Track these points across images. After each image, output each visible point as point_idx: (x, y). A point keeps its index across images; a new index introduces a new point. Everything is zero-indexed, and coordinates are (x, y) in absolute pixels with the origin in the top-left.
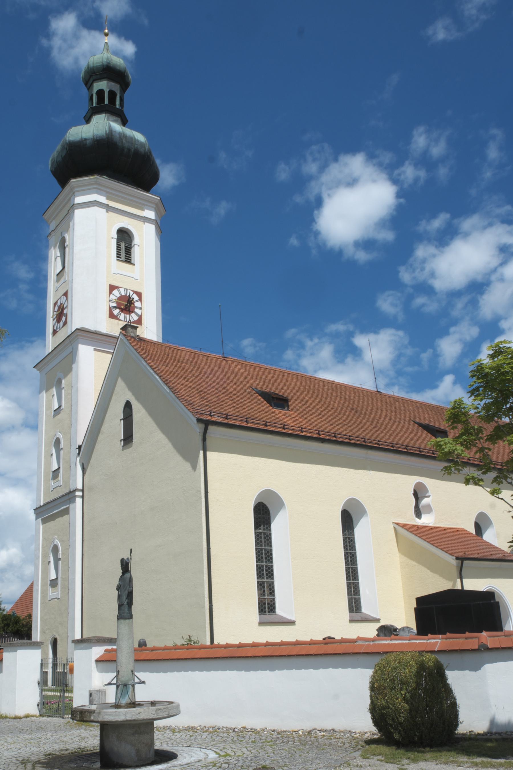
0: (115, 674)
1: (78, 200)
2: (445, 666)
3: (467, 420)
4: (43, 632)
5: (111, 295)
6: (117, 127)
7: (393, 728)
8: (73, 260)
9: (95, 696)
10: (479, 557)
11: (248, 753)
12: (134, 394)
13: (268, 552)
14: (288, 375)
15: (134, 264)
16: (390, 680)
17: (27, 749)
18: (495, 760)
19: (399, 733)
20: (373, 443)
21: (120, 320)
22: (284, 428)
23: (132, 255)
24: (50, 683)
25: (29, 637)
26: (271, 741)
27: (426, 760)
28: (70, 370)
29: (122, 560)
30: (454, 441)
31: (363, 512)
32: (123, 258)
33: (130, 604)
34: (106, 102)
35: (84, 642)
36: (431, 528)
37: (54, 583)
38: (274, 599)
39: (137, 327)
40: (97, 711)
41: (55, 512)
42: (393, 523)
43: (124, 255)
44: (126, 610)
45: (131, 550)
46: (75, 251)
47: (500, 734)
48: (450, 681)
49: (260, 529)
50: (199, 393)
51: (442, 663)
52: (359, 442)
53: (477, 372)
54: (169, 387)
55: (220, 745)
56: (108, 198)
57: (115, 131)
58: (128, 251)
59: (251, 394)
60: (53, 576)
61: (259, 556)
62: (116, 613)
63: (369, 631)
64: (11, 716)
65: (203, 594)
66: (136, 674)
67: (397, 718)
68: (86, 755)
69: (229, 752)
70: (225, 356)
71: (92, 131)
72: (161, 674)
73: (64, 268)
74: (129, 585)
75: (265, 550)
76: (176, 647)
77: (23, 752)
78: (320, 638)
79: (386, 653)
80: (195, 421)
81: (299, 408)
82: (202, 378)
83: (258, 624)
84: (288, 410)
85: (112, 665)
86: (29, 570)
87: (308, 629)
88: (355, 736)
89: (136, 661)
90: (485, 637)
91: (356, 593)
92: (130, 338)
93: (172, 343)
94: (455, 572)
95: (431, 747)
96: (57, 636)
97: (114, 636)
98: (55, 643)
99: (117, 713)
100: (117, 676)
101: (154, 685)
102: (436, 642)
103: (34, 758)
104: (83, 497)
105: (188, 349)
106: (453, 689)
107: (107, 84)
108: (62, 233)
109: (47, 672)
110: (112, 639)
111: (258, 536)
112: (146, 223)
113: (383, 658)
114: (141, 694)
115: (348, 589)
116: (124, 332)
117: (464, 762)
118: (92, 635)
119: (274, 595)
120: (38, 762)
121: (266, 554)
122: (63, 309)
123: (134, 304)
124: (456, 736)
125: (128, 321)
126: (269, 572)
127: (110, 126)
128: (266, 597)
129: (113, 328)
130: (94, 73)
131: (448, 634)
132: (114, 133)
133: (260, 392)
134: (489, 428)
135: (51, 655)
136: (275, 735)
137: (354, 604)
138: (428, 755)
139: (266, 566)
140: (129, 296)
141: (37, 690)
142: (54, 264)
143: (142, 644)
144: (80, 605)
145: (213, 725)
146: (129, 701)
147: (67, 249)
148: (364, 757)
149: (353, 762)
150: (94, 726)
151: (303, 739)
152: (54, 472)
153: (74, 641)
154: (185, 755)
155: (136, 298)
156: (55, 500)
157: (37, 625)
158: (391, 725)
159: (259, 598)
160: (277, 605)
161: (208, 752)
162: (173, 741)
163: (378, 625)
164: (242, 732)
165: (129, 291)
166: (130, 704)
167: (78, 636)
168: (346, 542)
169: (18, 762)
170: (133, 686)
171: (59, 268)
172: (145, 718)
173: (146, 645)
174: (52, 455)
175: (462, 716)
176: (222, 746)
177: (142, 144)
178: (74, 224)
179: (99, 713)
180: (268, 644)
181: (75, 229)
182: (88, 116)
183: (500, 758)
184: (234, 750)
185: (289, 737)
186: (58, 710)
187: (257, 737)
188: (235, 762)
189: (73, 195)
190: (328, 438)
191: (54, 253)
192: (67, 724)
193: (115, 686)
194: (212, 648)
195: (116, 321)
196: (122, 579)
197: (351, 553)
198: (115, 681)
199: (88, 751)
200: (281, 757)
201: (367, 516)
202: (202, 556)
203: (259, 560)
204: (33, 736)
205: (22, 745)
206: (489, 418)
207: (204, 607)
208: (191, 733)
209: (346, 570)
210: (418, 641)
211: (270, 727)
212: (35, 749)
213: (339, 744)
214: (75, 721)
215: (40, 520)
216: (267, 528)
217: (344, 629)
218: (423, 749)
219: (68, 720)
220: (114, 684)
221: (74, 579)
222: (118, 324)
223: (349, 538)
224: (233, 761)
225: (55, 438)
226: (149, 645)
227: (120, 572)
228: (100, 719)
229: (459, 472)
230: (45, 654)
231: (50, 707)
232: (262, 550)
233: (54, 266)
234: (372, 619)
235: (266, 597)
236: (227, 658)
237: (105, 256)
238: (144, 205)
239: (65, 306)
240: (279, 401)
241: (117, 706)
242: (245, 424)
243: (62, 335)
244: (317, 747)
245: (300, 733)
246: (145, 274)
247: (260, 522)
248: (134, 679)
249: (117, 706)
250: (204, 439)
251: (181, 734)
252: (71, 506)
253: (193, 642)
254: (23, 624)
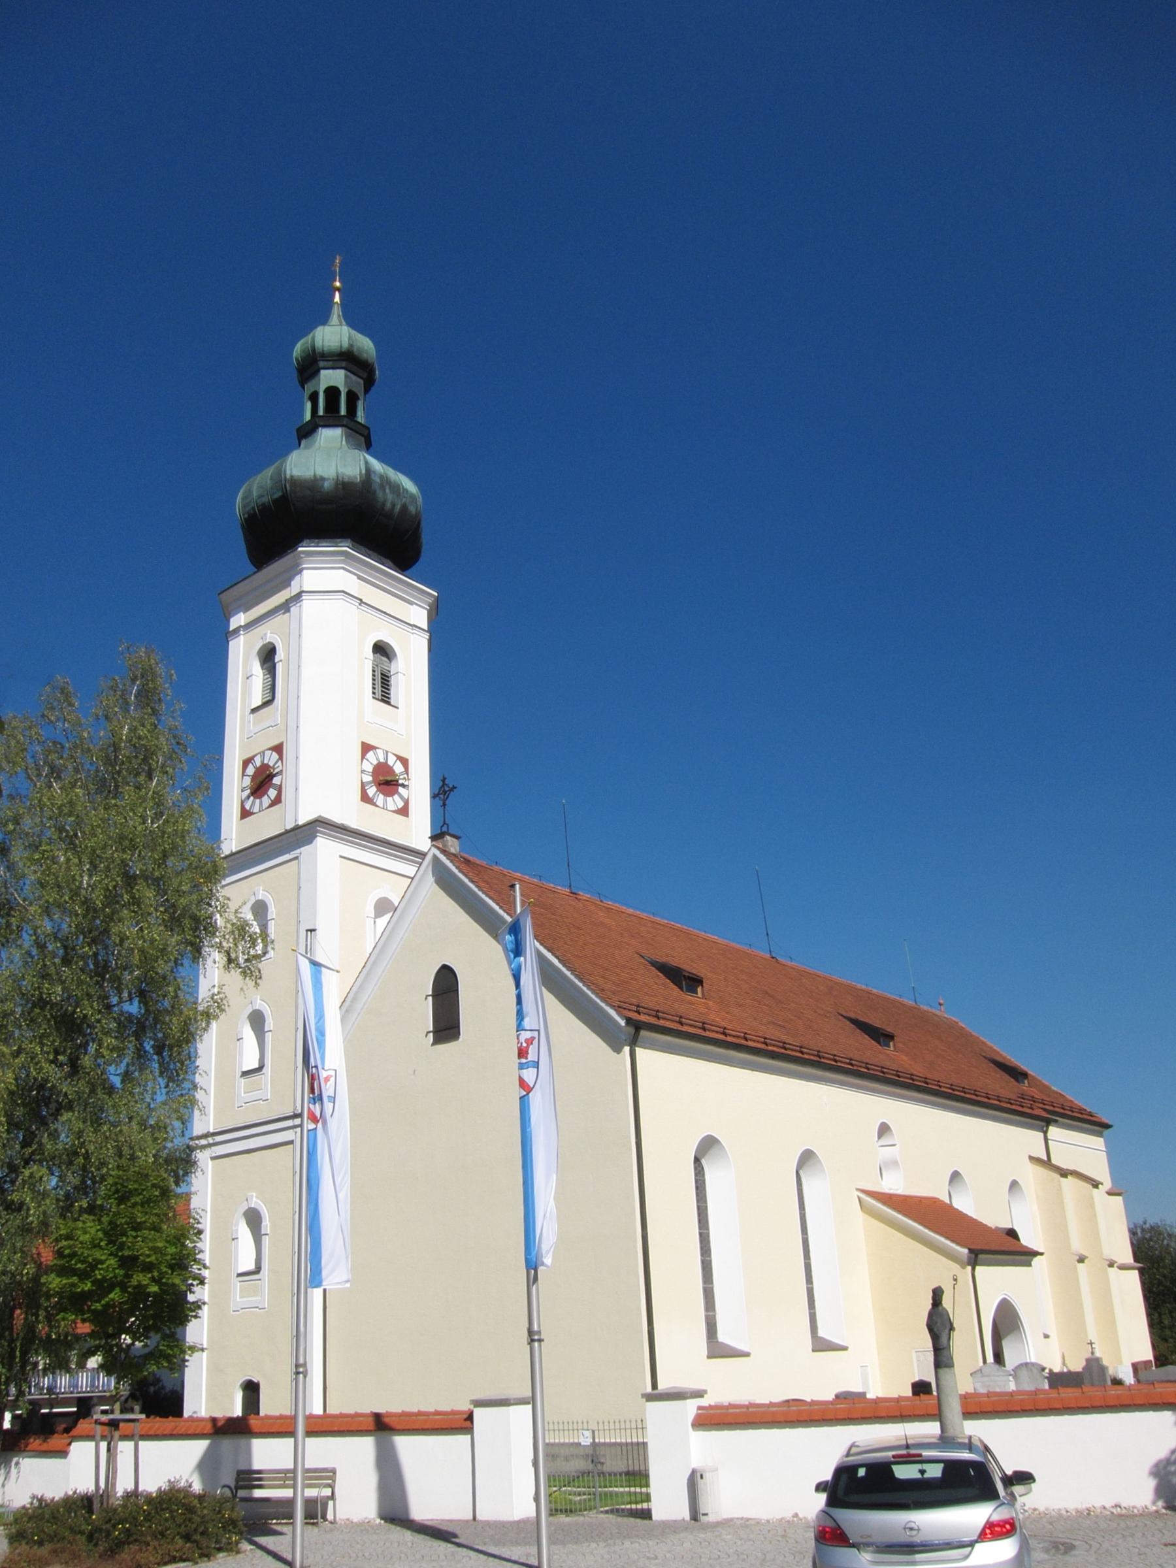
21: (375, 805)
32: (378, 695)
34: (343, 412)
42: (858, 1189)
107: (346, 376)
177: (413, 498)
246: (408, 729)
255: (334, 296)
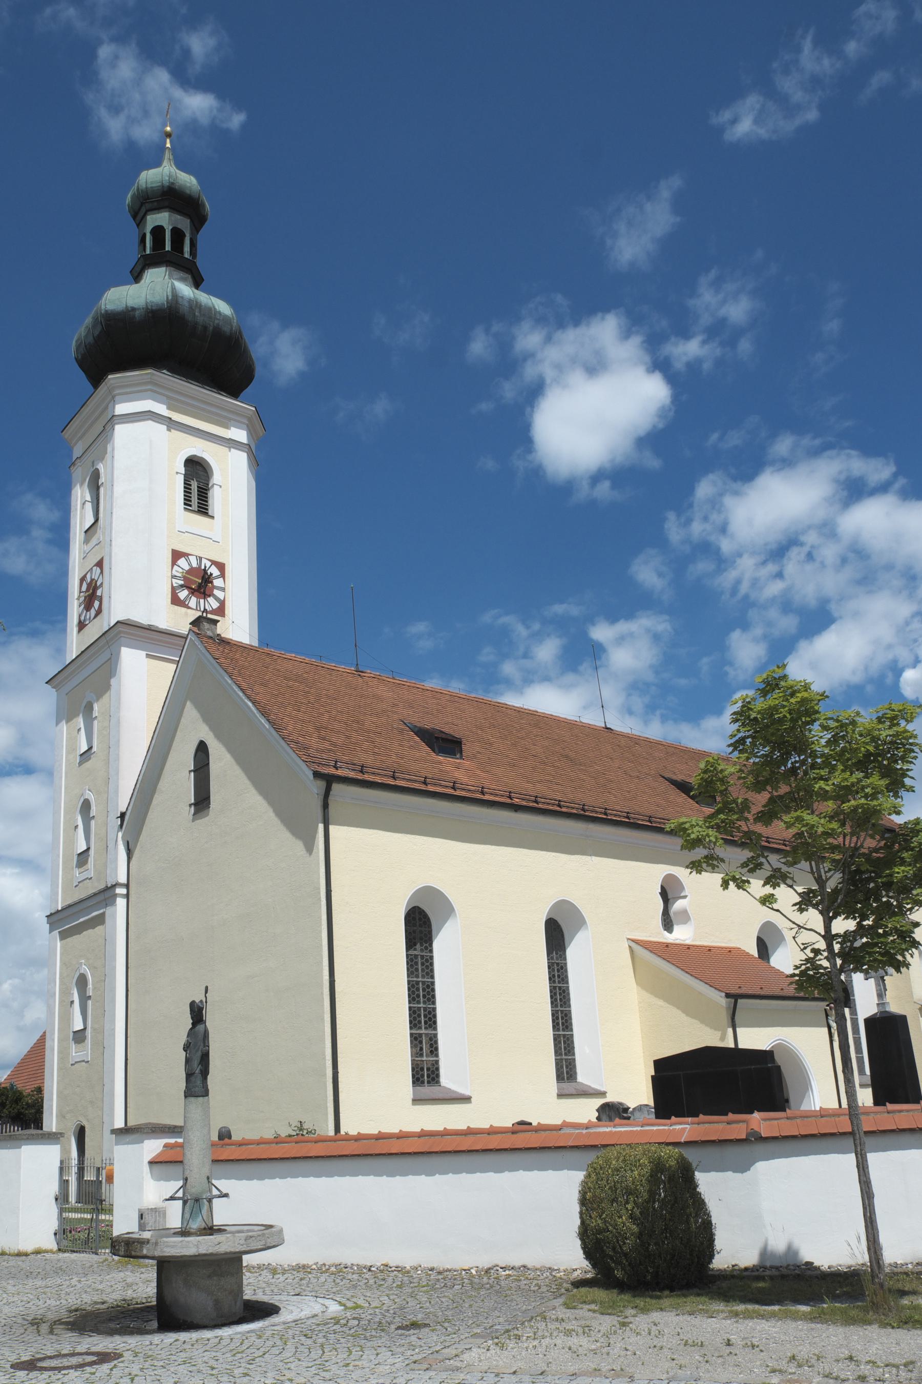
0: (181, 1183)
1: (121, 408)
2: (694, 1165)
3: (726, 789)
4: (61, 1116)
5: (175, 567)
6: (185, 290)
7: (614, 1262)
8: (112, 509)
9: (149, 1220)
10: (762, 993)
11: (391, 1303)
12: (212, 728)
13: (428, 986)
14: (461, 701)
15: (213, 517)
16: (610, 1188)
17: (40, 1303)
18: (766, 1308)
19: (623, 1269)
20: (597, 812)
21: (189, 608)
22: (454, 788)
23: (210, 502)
24: (73, 1198)
25: (39, 1124)
26: (427, 1285)
27: (661, 1310)
28: (108, 687)
29: (192, 1004)
30: (705, 822)
31: (580, 922)
32: (195, 506)
33: (205, 1072)
34: (168, 247)
35: (127, 1132)
36: (689, 947)
37: (79, 1037)
38: (437, 1062)
39: (217, 621)
40: (153, 1241)
41: (81, 920)
42: (628, 939)
43: (197, 501)
44: (199, 1082)
45: (207, 988)
46: (115, 494)
47: (777, 1268)
48: (702, 1188)
49: (415, 950)
50: (318, 729)
51: (690, 1160)
52: (574, 811)
53: (741, 716)
54: (268, 720)
55: (347, 1292)
56: (169, 408)
57: (182, 297)
58: (203, 494)
59: (401, 731)
60: (78, 1025)
61: (413, 992)
62: (183, 1085)
63: (585, 1111)
64: (12, 1252)
65: (324, 1054)
66: (214, 1182)
67: (620, 1247)
68: (134, 1310)
69: (361, 1302)
70: (360, 669)
71: (143, 296)
72: (255, 1182)
73: (97, 520)
74: (204, 1043)
75: (424, 983)
76: (277, 1140)
77: (34, 1308)
78: (508, 1124)
79: (605, 1146)
80: (311, 776)
81: (479, 756)
82: (323, 706)
83: (411, 1102)
84: (461, 758)
85: (177, 1169)
86: (36, 1013)
87: (491, 1110)
88: (558, 1275)
89: (215, 1161)
90: (758, 1121)
91: (569, 1051)
92: (205, 639)
93: (275, 648)
94: (724, 1017)
95: (672, 1290)
96: (85, 1123)
97: (180, 1123)
98: (81, 1134)
99: (184, 1243)
100: (184, 1186)
101: (242, 1201)
102: (682, 1128)
103: (51, 1316)
104: (127, 896)
105: (300, 658)
106: (706, 1201)
107: (170, 216)
108: (93, 463)
109: (67, 1181)
110: (175, 1127)
111: (412, 960)
112: (232, 450)
113: (599, 1154)
114: (222, 1213)
115: (555, 1045)
116: (195, 629)
117: (718, 1311)
118: (142, 1121)
119: (437, 1055)
120: (59, 1322)
121: (424, 990)
122: (95, 588)
123: (212, 582)
124: (710, 1273)
125: (202, 609)
126: (430, 1019)
127: (174, 289)
128: (425, 1058)
129: (178, 621)
130: (148, 199)
131: (701, 1116)
132: (180, 300)
133: (416, 729)
134: (760, 800)
135: (74, 1153)
136: (434, 1276)
137: (566, 1069)
138: (666, 1302)
139: (425, 1009)
140: (205, 570)
141: (54, 1210)
142: (81, 512)
143: (225, 1135)
144: (120, 1072)
145: (337, 1262)
146: (203, 1225)
147: (102, 490)
148: (567, 1306)
149: (552, 1314)
150: (147, 1266)
151: (476, 1281)
152: (79, 855)
153: (114, 1131)
154: (290, 1308)
155: (214, 571)
156: (81, 901)
157: (52, 1106)
158: (611, 1258)
159: (412, 1061)
160: (442, 1071)
161: (327, 1302)
162: (272, 1287)
163: (600, 1102)
164: (382, 1271)
165: (204, 561)
166: (205, 1229)
167: (119, 1123)
168: (553, 970)
169: (26, 1323)
170: (210, 1201)
171: (90, 520)
172: (228, 1251)
173: (230, 1137)
174: (76, 827)
175: (720, 1242)
176: (349, 1294)
177: (226, 317)
178: (113, 450)
179: (156, 1244)
180: (423, 1134)
181: (115, 457)
182: (138, 269)
183: (774, 1304)
184: (369, 1299)
185: (455, 1279)
186: (87, 1241)
187: (406, 1279)
188: (369, 1317)
189: (113, 400)
190: (524, 803)
191: (80, 494)
192: (102, 1263)
193: (181, 1202)
194: (335, 1141)
195: (184, 610)
196: (191, 1033)
197: (560, 988)
198: (180, 1194)
199: (137, 1304)
200: (440, 1308)
201: (587, 928)
202: (322, 993)
203: (414, 999)
204: (49, 1282)
205: (32, 1297)
206: (759, 786)
207: (325, 1075)
208: (301, 1275)
209: (553, 1015)
210: (655, 1128)
211: (427, 1264)
212: (52, 1302)
213: (532, 1288)
214: (116, 1258)
215: (56, 933)
216: (426, 948)
217: (548, 1108)
218: (659, 1293)
219: (104, 1257)
220: (179, 1199)
221: (114, 1029)
222: (186, 614)
223: (558, 964)
224: (366, 1316)
225: (82, 800)
226: (235, 1137)
227: (187, 1022)
228: (157, 1253)
229: (713, 869)
230: (65, 1151)
231: (68, 1237)
232: (417, 983)
233: (81, 517)
234: (592, 1092)
235: (425, 1058)
236: (359, 1155)
237: (165, 502)
238: (230, 419)
239: (98, 584)
240: (446, 744)
241: (184, 1233)
242: (391, 782)
243: (94, 631)
244: (497, 1292)
245: (473, 1271)
246: (230, 534)
247: (414, 938)
248: (210, 1191)
249: (184, 1233)
250: (325, 806)
251: (286, 1276)
252: (109, 911)
253: (305, 1132)
254: (27, 1104)
255: (165, 143)
